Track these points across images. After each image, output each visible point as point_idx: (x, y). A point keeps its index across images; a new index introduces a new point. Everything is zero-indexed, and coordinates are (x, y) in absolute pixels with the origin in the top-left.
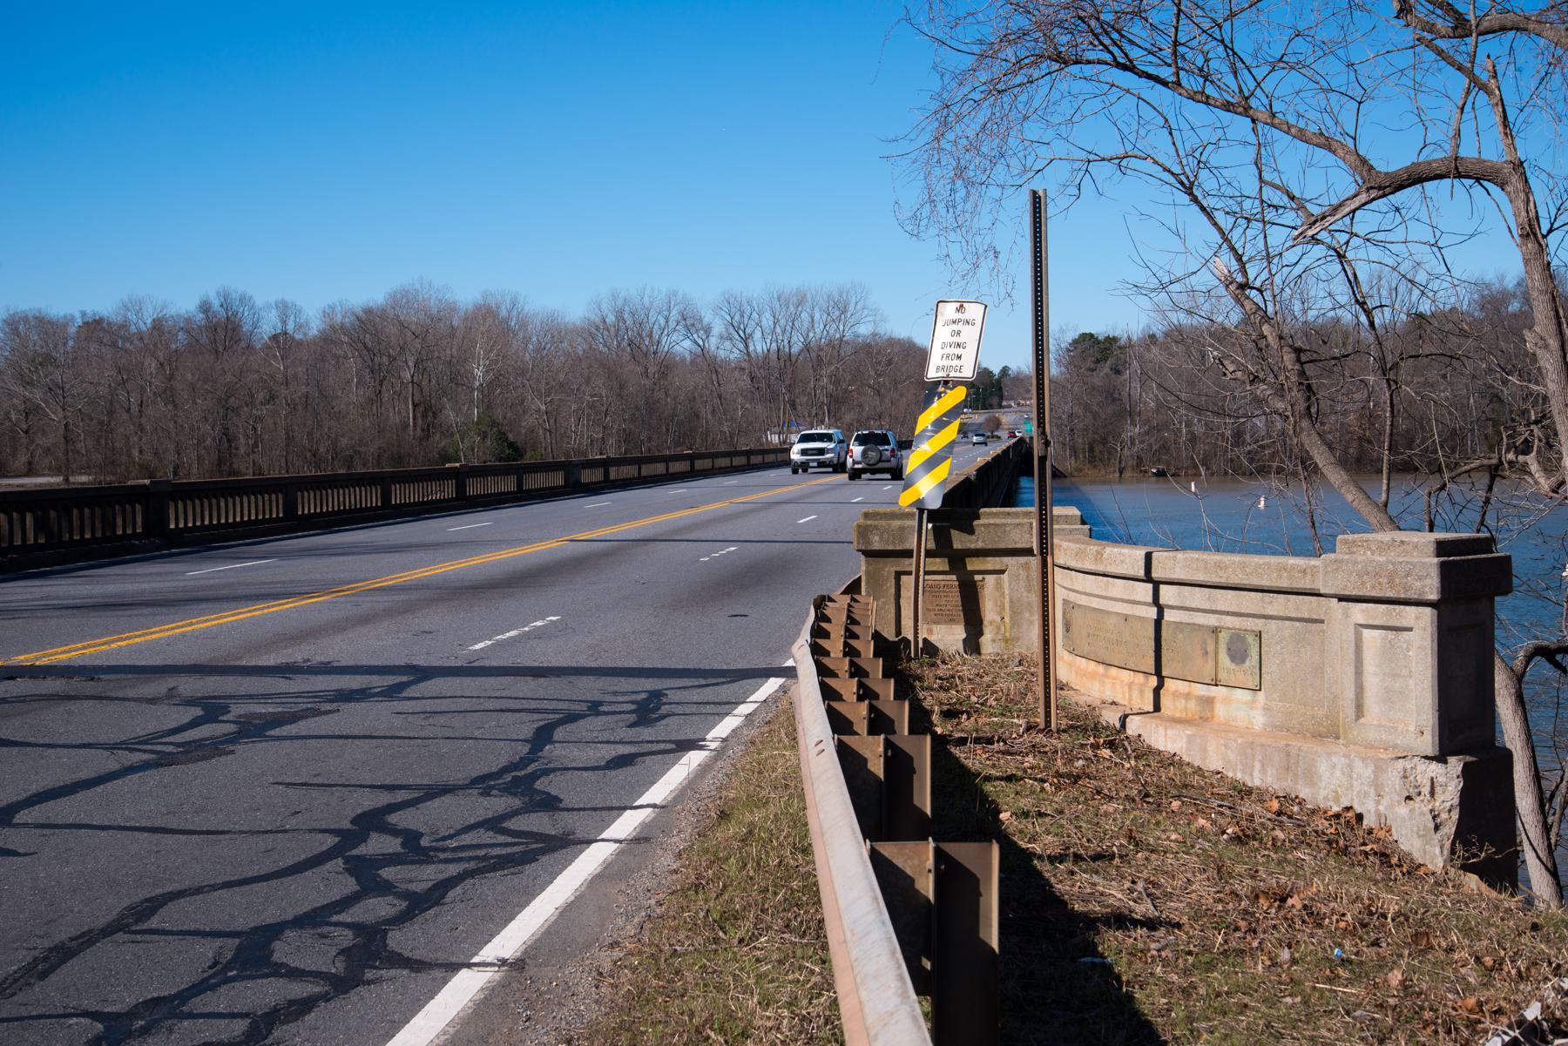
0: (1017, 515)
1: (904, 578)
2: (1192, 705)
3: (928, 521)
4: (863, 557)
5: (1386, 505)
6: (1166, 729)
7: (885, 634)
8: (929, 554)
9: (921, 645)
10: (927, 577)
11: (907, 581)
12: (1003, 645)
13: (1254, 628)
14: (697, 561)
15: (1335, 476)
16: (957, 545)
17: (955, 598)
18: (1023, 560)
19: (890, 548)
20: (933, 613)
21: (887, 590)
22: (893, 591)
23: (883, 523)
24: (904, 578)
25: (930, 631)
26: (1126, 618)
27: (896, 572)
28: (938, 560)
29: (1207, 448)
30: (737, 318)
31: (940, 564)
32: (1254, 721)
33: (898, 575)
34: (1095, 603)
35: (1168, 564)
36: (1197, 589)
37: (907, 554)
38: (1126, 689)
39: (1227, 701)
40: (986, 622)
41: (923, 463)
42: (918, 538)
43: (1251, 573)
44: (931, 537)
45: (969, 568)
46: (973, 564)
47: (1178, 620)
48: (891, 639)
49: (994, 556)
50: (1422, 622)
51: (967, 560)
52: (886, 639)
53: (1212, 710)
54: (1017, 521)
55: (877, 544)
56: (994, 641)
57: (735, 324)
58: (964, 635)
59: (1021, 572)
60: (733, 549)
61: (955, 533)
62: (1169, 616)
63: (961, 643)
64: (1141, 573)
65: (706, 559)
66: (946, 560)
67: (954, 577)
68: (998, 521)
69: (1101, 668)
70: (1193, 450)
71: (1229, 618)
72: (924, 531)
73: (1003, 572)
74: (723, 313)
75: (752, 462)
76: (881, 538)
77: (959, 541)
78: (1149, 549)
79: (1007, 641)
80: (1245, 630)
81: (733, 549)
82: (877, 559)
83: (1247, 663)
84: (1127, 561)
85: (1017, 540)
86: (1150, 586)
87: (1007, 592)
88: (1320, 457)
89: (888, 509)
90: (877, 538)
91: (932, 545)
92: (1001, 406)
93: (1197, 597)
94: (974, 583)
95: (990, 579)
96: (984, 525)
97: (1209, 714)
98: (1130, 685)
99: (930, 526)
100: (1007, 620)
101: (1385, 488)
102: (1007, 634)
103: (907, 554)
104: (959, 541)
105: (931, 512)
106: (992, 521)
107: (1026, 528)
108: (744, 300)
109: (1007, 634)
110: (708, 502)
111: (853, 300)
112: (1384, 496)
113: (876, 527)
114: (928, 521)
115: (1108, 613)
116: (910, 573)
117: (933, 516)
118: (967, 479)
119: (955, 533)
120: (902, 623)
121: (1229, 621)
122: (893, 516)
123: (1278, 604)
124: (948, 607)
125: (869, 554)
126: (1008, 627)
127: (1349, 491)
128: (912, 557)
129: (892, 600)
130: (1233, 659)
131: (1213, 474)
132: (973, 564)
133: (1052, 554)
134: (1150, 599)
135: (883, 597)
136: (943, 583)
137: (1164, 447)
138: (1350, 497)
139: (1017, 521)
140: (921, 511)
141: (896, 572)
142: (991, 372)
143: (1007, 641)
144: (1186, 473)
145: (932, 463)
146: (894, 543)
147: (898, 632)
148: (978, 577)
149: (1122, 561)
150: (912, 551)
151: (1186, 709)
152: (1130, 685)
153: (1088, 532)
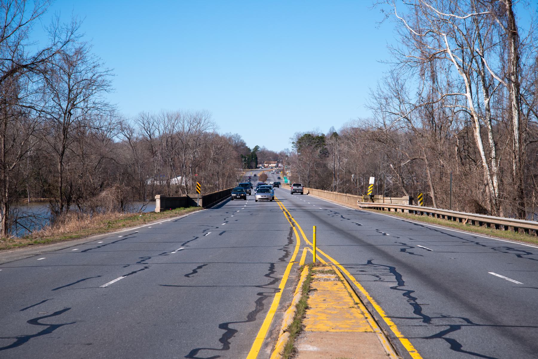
30: (147, 125)
35: (392, 198)
42: (369, 198)
46: (374, 200)
50: (408, 201)
55: (365, 198)
57: (146, 128)
74: (140, 122)
77: (373, 198)
92: (256, 168)
93: (394, 201)
104: (373, 198)
108: (150, 116)
111: (203, 118)
117: (371, 196)
123: (399, 201)
132: (374, 200)
142: (249, 149)
145: (370, 191)
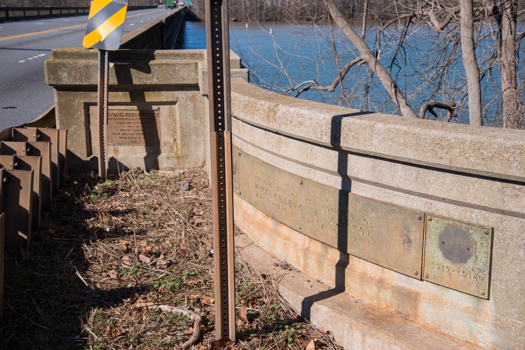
0: (184, 56)
1: (92, 108)
2: (387, 296)
3: (110, 60)
4: (55, 91)
5: (364, 38)
6: (364, 335)
7: (78, 154)
8: (111, 88)
9: (107, 167)
10: (110, 107)
11: (95, 111)
12: (176, 161)
13: (482, 223)
14: (18, 62)
15: (341, 22)
16: (136, 82)
17: (136, 125)
18: (190, 93)
19: (78, 83)
20: (118, 136)
21: (78, 118)
22: (83, 119)
23: (70, 61)
24: (92, 108)
25: (116, 151)
26: (302, 182)
27: (85, 103)
28: (120, 93)
29: (251, 11)
31: (123, 96)
32: (479, 336)
33: (87, 106)
34: (264, 157)
36: (400, 166)
37: (93, 88)
38: (301, 255)
39: (436, 301)
40: (162, 144)
41: (103, 9)
43: (491, 158)
44: (113, 74)
45: (148, 100)
46: (150, 97)
47: (369, 196)
48: (84, 159)
49: (167, 90)
51: (146, 93)
52: (79, 159)
53: (415, 308)
54: (184, 61)
55: (66, 80)
56: (168, 158)
58: (145, 154)
59: (189, 103)
60: (43, 55)
61: (133, 71)
62: (356, 189)
63: (143, 160)
64: (327, 140)
65: (31, 59)
66: (128, 93)
67: (135, 107)
68: (169, 61)
69: (270, 222)
70: (246, 12)
71: (443, 205)
72: (106, 70)
73: (174, 103)
75: (23, 12)
76: (69, 74)
78: (340, 110)
79: (178, 158)
80: (469, 224)
81: (43, 55)
82: (68, 93)
83: (470, 263)
84: (308, 123)
85: (185, 77)
86: (335, 154)
87: (178, 119)
88: (334, 12)
89: (75, 50)
90: (65, 75)
91: (114, 81)
94: (152, 113)
95: (164, 109)
96: (158, 65)
97: (410, 312)
98: (306, 251)
99: (112, 65)
100: (179, 141)
101: (363, 29)
102: (179, 153)
103: (93, 88)
105: (110, 52)
106: (164, 61)
107: (192, 67)
109: (179, 153)
110: (49, 29)
112: (363, 33)
113: (64, 65)
114: (110, 60)
115: (280, 171)
116: (95, 104)
117: (113, 56)
118: (161, 22)
119: (133, 71)
120: (93, 145)
121: (442, 209)
122: (79, 55)
124: (131, 132)
125: (61, 88)
126: (179, 146)
127: (347, 30)
128: (96, 91)
129: (83, 127)
130: (448, 254)
131: (253, 21)
132: (150, 97)
133: (230, 129)
134: (335, 168)
135: (75, 124)
136: (126, 112)
137: (236, 11)
138: (347, 34)
139: (184, 61)
140: (103, 52)
141: (85, 103)
143: (178, 158)
144: (244, 21)
146: (80, 79)
147: (90, 152)
148: (154, 107)
149: (301, 124)
150: (96, 86)
151: (378, 297)
152: (306, 251)
153: (246, 75)
